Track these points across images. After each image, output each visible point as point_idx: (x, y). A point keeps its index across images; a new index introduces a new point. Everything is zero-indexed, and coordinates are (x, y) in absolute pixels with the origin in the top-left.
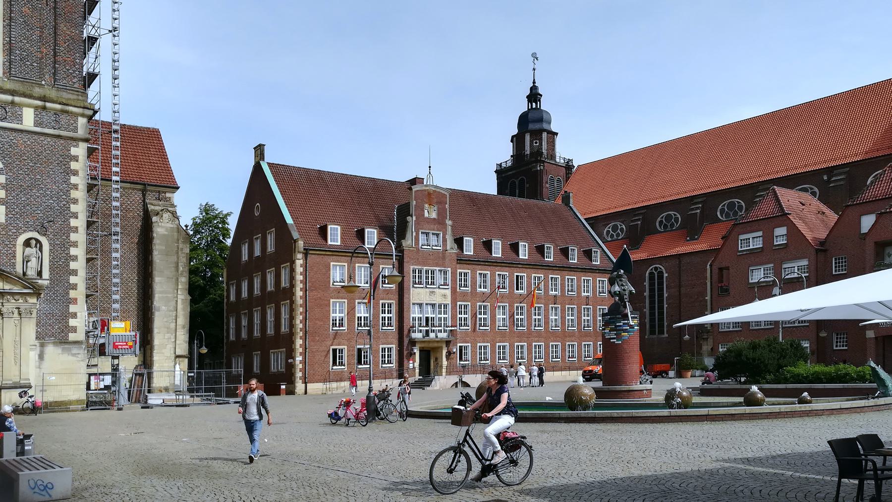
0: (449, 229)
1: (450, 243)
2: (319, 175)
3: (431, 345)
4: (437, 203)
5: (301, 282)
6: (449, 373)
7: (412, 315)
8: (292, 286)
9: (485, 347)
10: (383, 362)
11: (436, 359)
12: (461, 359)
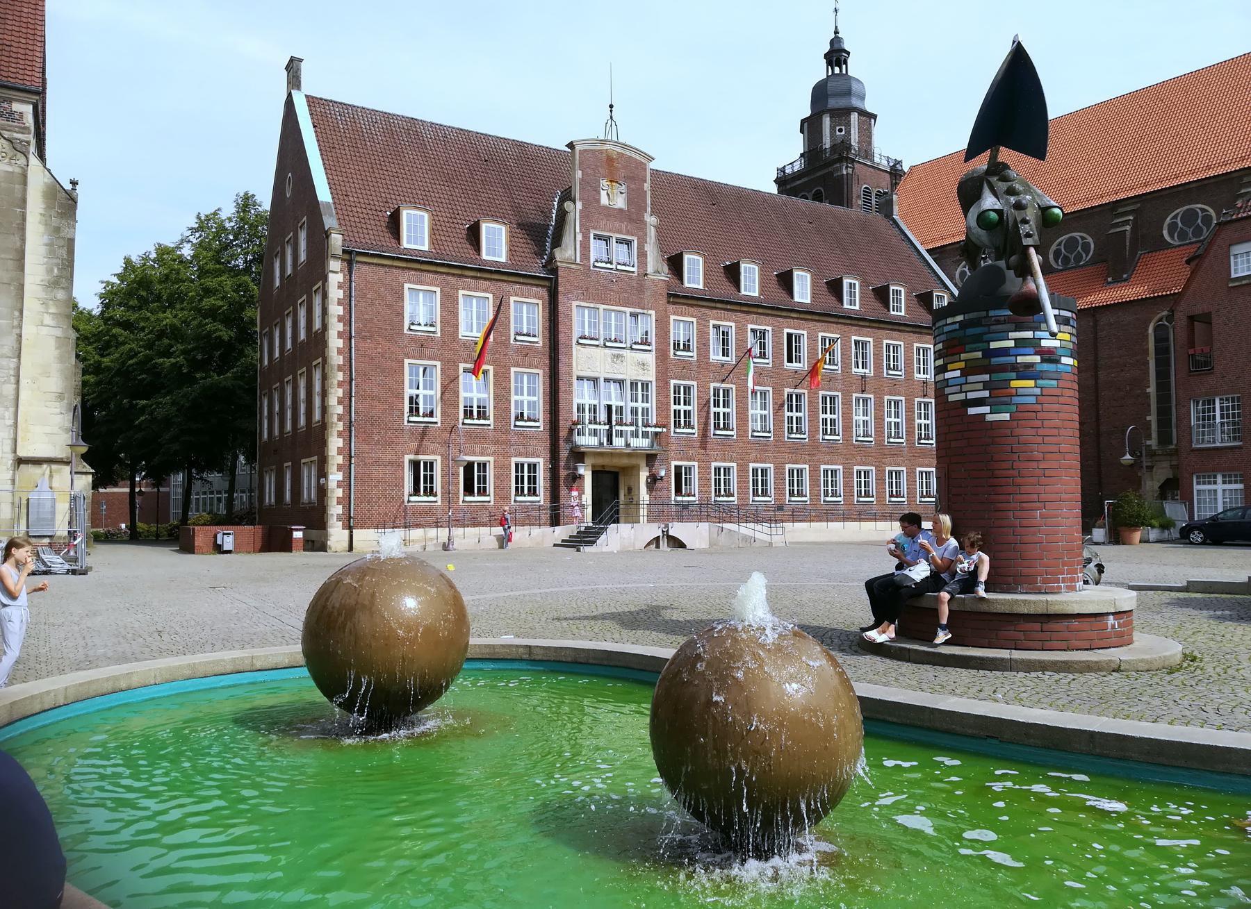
0: (652, 232)
3: (617, 462)
4: (627, 178)
5: (340, 319)
7: (576, 401)
8: (325, 326)
11: (630, 490)
12: (678, 491)
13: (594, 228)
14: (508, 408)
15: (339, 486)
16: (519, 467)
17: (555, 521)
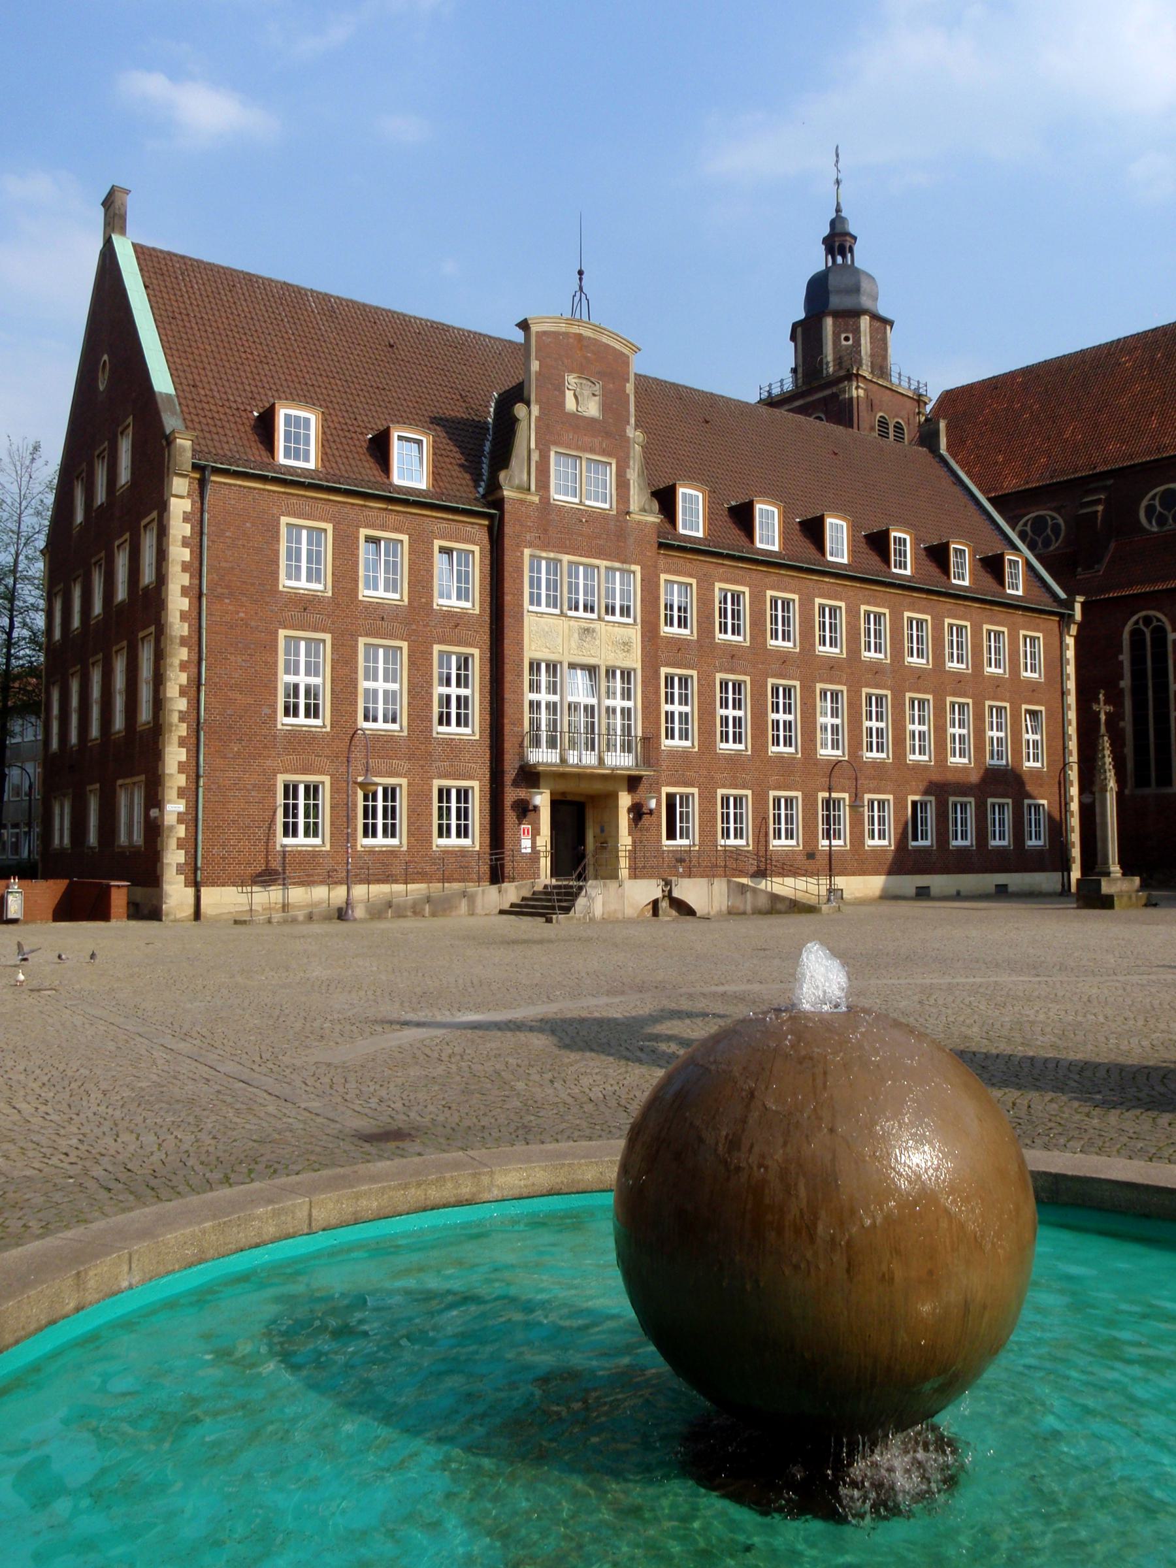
1: (638, 498)
2: (288, 300)
3: (586, 787)
4: (601, 375)
5: (185, 567)
6: (635, 874)
8: (161, 579)
9: (738, 800)
10: (444, 831)
13: (556, 444)
14: (429, 705)
15: (180, 821)
16: (444, 794)
17: (497, 876)
